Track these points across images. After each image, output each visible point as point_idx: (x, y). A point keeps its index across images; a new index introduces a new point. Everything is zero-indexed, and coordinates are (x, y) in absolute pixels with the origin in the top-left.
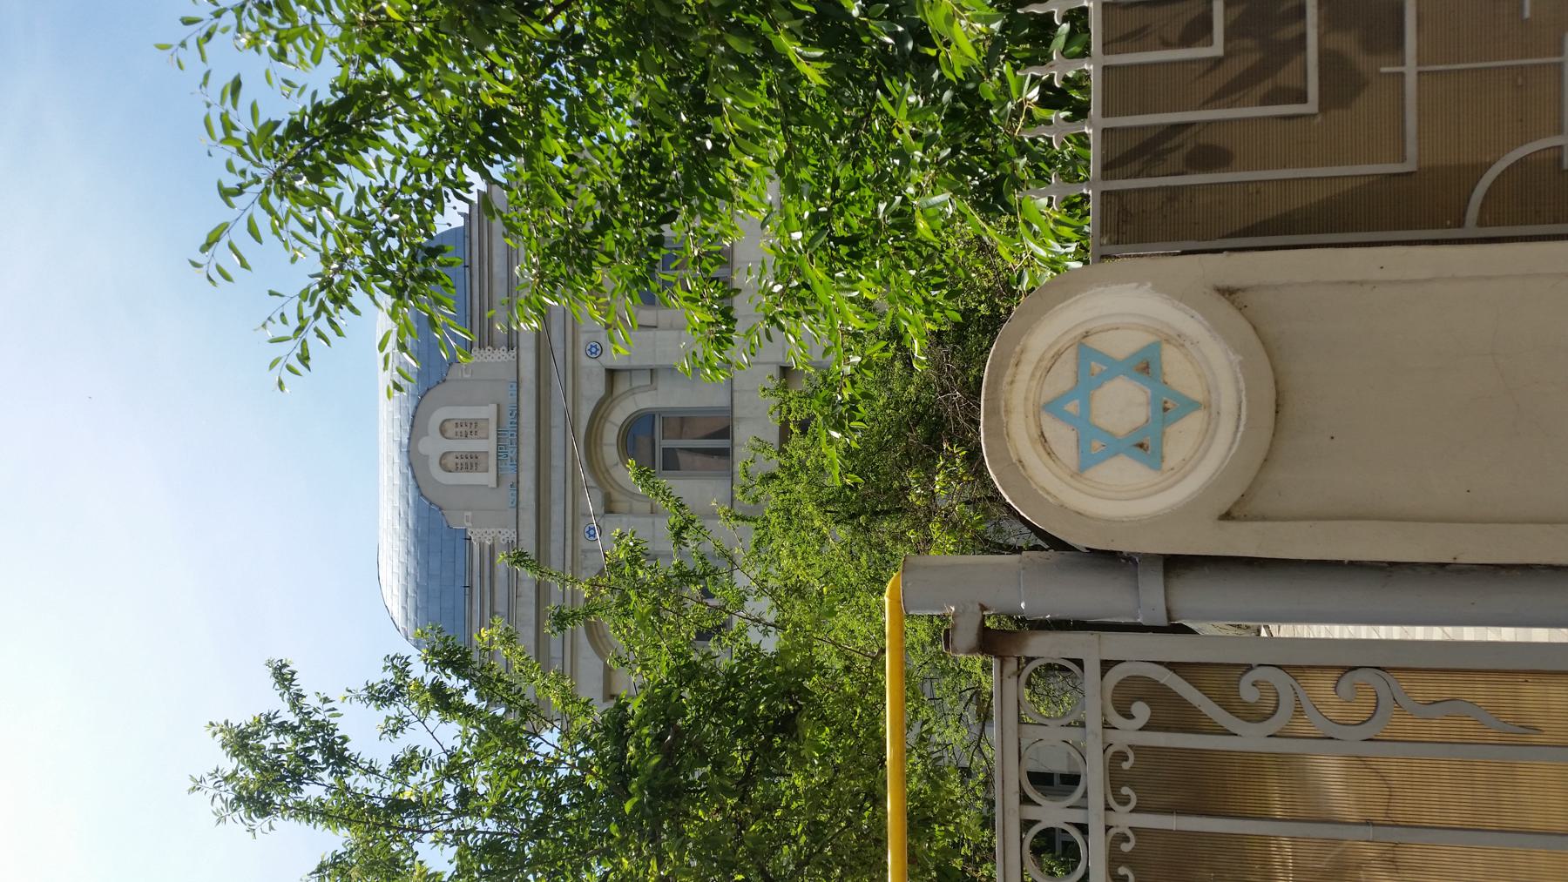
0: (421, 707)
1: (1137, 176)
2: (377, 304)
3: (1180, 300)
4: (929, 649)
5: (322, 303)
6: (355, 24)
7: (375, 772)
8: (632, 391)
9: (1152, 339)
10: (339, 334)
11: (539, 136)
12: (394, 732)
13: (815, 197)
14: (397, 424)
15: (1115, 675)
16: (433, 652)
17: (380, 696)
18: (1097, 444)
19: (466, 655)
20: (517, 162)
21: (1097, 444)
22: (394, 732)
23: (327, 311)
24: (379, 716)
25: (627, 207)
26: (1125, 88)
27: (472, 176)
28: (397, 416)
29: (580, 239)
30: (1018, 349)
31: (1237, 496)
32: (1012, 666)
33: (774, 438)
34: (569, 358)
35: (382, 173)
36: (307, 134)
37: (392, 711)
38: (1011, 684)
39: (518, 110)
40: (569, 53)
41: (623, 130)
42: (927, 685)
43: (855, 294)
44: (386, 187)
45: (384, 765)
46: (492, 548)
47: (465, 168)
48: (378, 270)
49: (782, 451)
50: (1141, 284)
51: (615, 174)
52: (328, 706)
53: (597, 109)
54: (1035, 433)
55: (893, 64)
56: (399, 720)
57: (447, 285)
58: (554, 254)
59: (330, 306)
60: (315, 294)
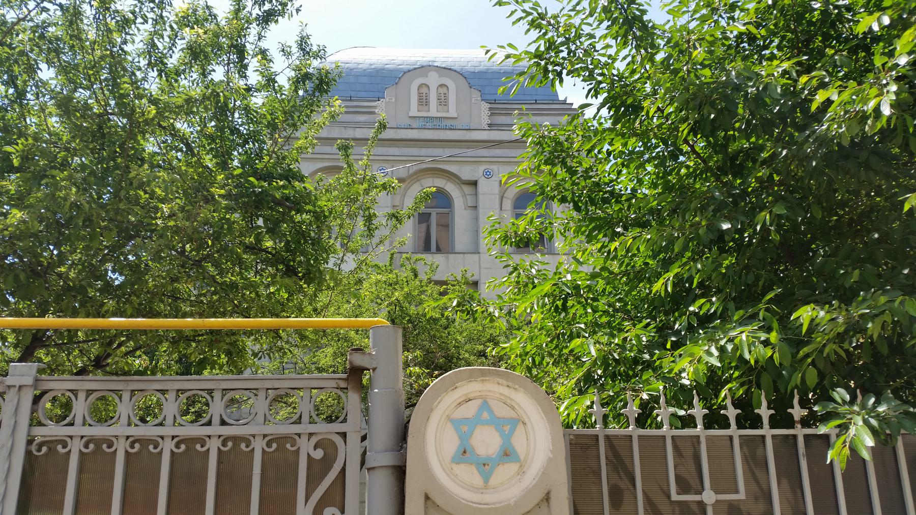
0: (297, 66)
1: (607, 458)
2: (529, 44)
3: (543, 473)
4: (313, 366)
5: (531, 14)
6: (688, 33)
7: (259, 39)
8: (464, 196)
9: (522, 458)
10: (514, 23)
11: (623, 135)
12: (283, 50)
13: (589, 288)
14: (446, 59)
15: (338, 440)
16: (328, 72)
17: (303, 43)
18: (465, 428)
19: (326, 92)
20: (608, 124)
21: (465, 428)
22: (283, 50)
23: (526, 16)
24: (292, 41)
25: (583, 184)
26: (654, 446)
27: (601, 98)
28: (450, 60)
29: (564, 158)
30: (517, 387)
31: (438, 503)
32: (343, 384)
33: (436, 278)
34: (483, 159)
35: (603, 48)
36: (629, 6)
37: (295, 49)
38: (333, 384)
39: (637, 124)
40: (669, 152)
41: (625, 184)
42: (292, 366)
43: (536, 307)
44: (595, 51)
45: (263, 44)
46: (373, 113)
47: (605, 95)
48: (551, 45)
49: (430, 281)
50: (552, 452)
51: (600, 179)
52: (294, 12)
53: (637, 168)
54: (471, 396)
55: (663, 330)
56: (289, 54)
57: (541, 82)
58: (556, 144)
59: (530, 18)
60: (536, 10)
